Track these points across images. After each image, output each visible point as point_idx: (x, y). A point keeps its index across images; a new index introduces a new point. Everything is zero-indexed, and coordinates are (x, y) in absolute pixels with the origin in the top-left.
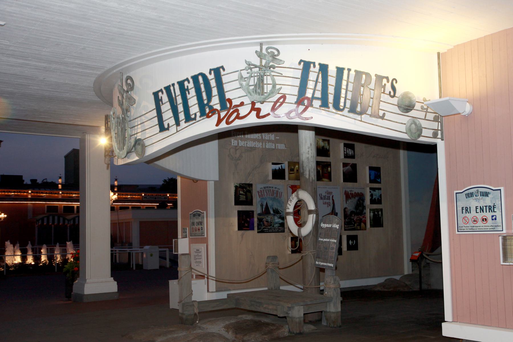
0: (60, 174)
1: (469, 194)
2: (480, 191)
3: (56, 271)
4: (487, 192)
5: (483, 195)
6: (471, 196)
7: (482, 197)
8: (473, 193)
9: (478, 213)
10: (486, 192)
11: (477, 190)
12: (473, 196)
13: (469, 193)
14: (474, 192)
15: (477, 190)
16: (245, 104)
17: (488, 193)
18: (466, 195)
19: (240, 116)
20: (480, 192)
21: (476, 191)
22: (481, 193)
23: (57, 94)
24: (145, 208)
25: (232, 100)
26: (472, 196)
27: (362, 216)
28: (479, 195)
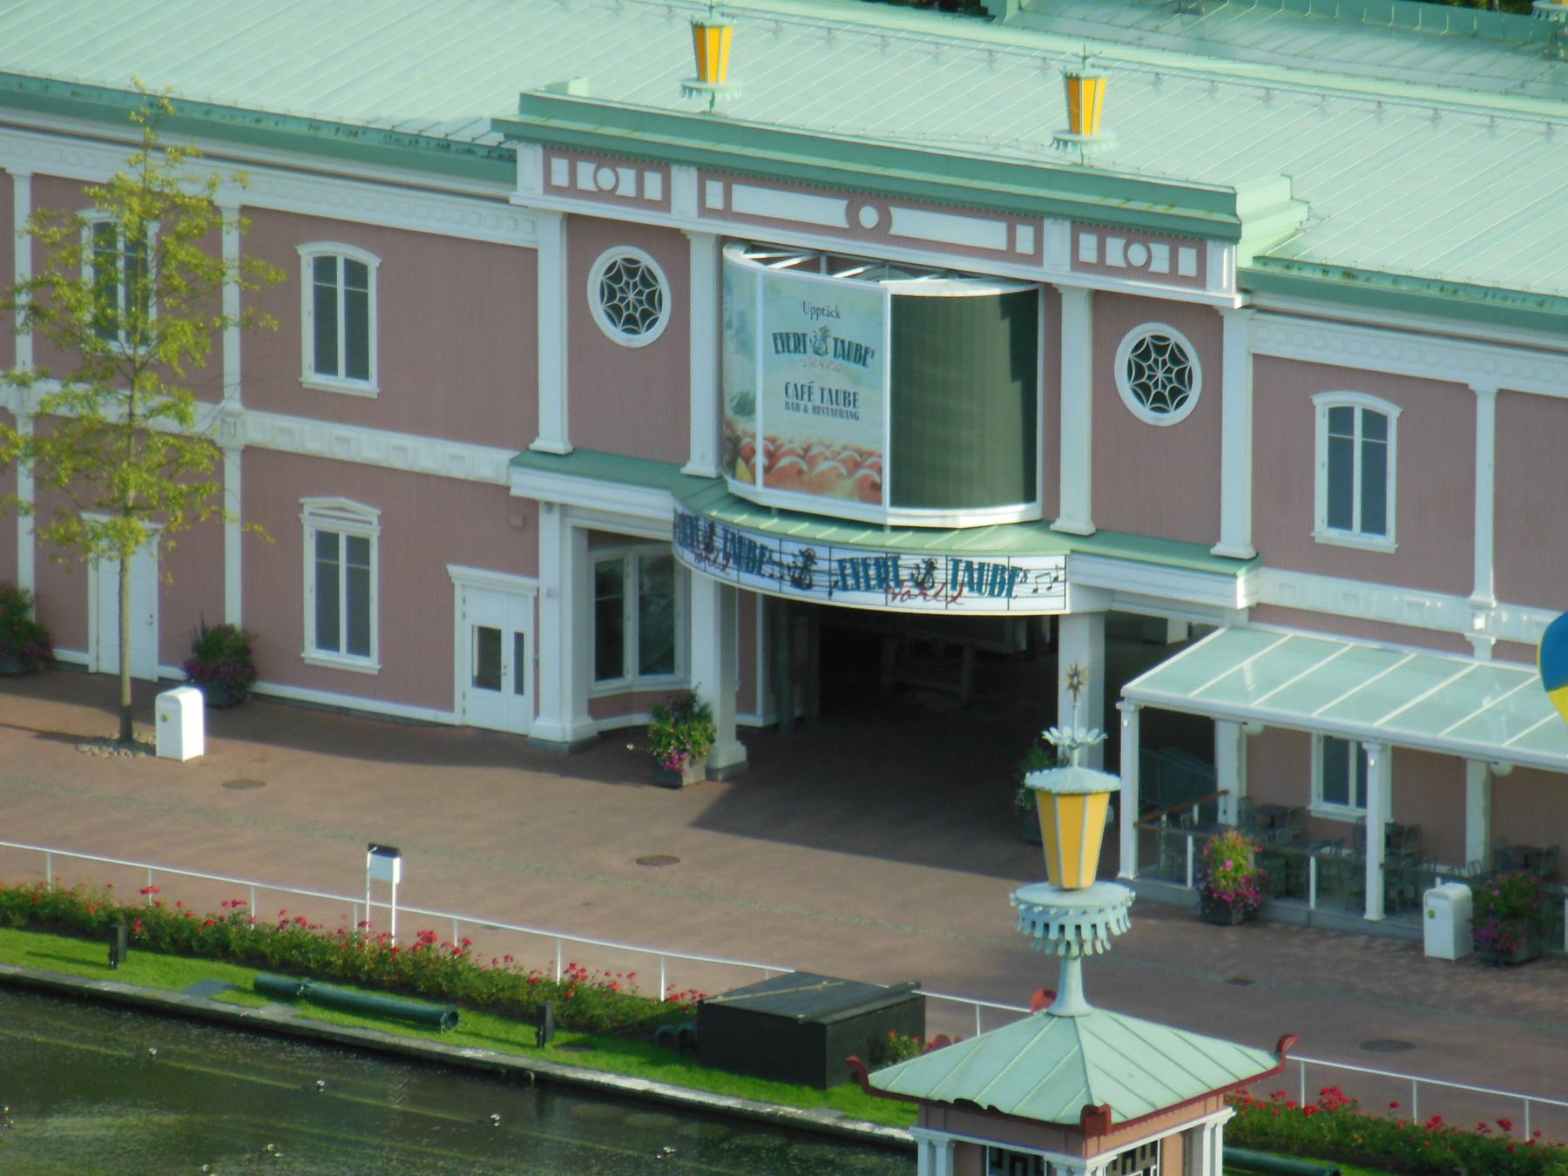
0: (1093, 922)
1: (788, 338)
2: (834, 333)
3: (1190, 840)
4: (852, 392)
5: (846, 356)
6: (796, 349)
7: (840, 361)
8: (804, 335)
9: (830, 593)
10: (857, 345)
11: (821, 330)
12: (805, 351)
13: (787, 334)
14: (813, 335)
15: (821, 330)
16: (1116, 1118)
17: (866, 352)
18: (775, 339)
19: (894, 231)
20: (836, 340)
21: (819, 333)
22: (839, 344)
23: (932, 140)
24: (1244, 618)
25: (707, 31)
26: (802, 349)
27: (11, 917)
28: (831, 351)
